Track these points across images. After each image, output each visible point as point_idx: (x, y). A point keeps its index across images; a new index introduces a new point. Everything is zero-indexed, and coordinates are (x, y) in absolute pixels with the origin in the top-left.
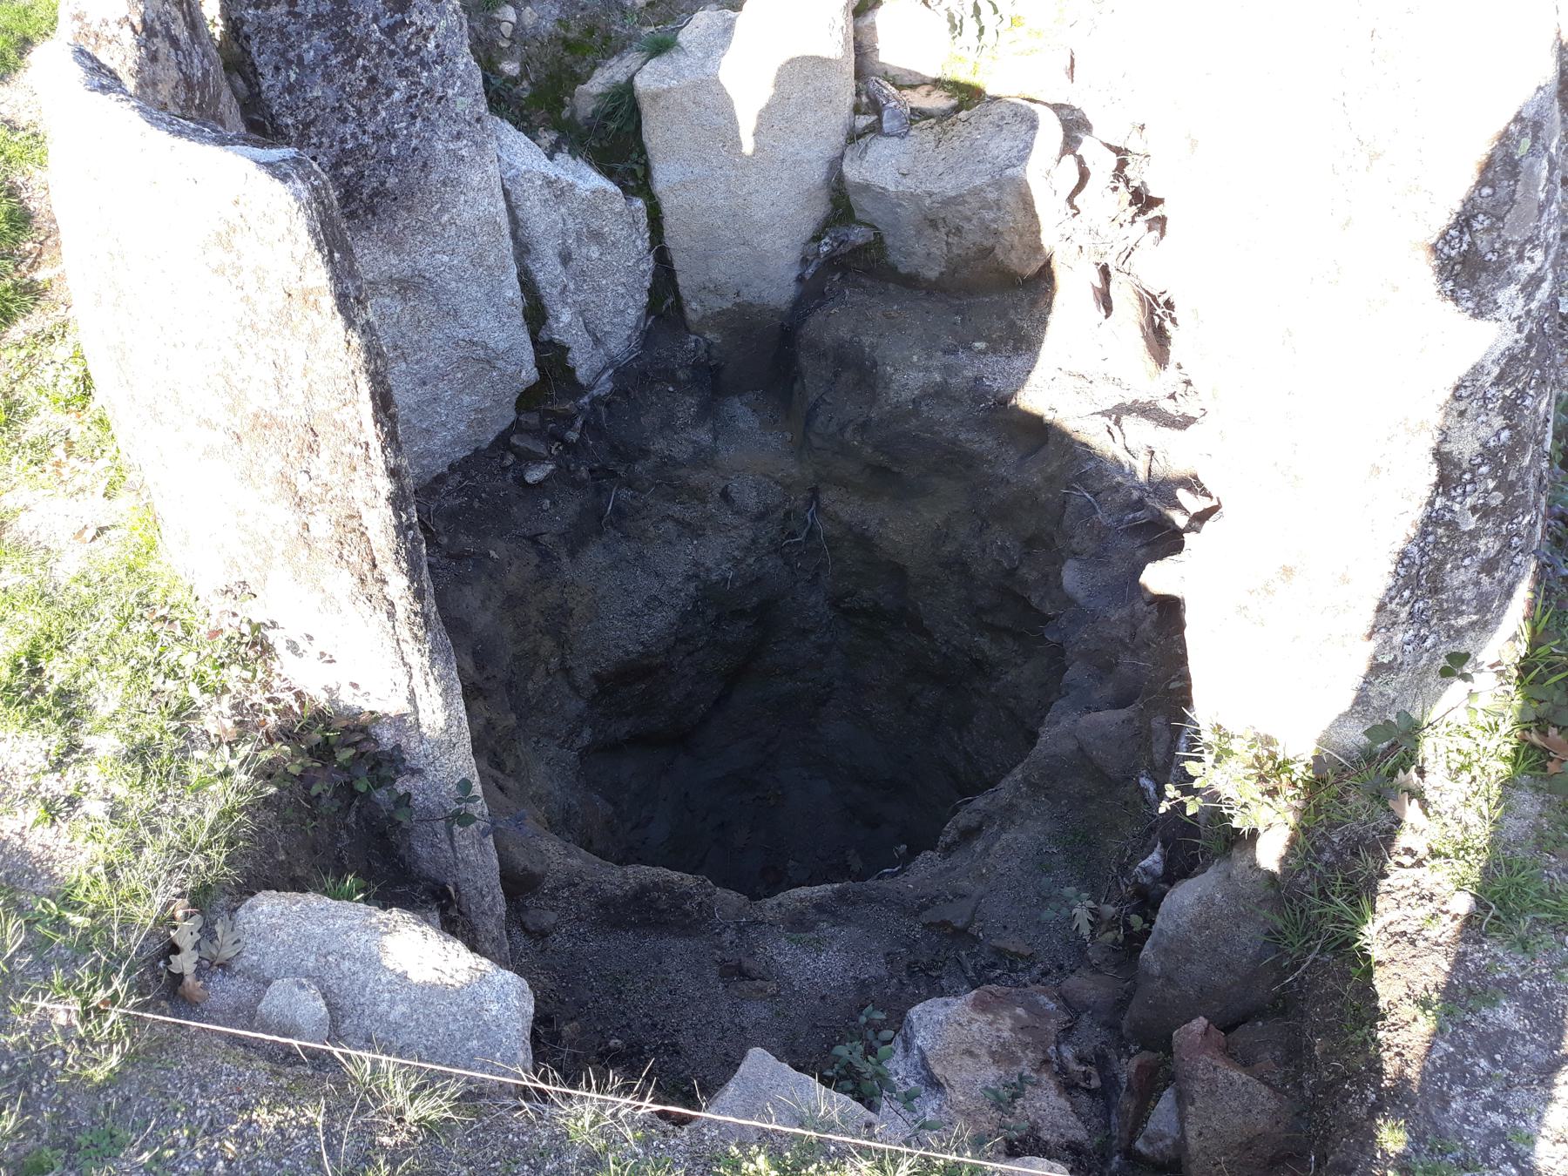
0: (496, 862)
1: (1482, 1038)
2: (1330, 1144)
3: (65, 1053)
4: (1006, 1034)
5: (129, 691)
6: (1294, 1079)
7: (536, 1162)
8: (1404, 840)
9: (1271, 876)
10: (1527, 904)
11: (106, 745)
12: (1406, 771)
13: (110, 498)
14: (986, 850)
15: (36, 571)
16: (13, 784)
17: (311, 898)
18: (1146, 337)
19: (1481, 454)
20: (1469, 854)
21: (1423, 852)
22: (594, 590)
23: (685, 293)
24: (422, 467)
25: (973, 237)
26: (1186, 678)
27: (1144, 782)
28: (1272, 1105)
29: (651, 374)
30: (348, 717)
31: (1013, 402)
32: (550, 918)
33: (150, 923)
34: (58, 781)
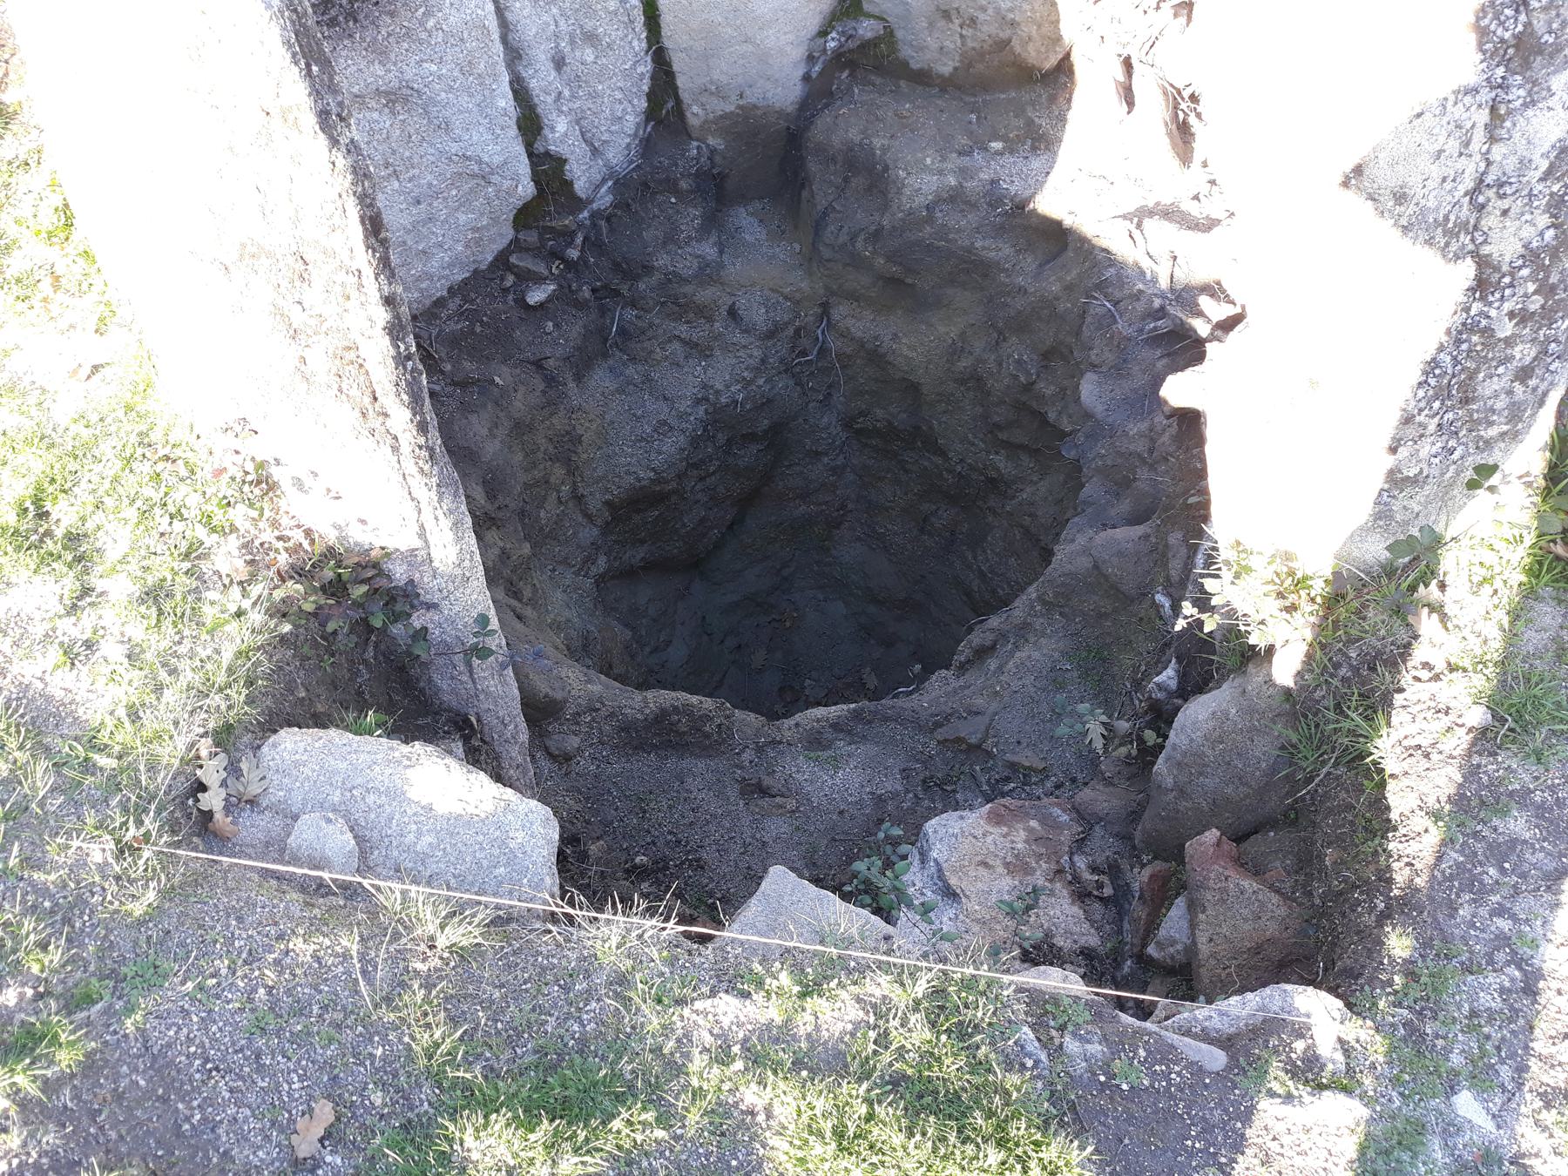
0: (516, 692)
1: (1492, 847)
2: (1339, 951)
3: (104, 889)
4: (1019, 846)
5: (138, 532)
6: (1304, 887)
7: (566, 983)
8: (1420, 653)
9: (1287, 692)
10: (1544, 716)
11: (119, 587)
12: (1426, 586)
13: (101, 334)
14: (1000, 669)
15: (34, 412)
16: (30, 628)
17: (333, 733)
18: (1170, 134)
19: (1523, 256)
20: (1487, 667)
21: (1440, 666)
22: (602, 416)
23: (685, 96)
24: (421, 291)
25: (989, 28)
26: (1204, 492)
27: (1159, 598)
28: (1283, 911)
29: (652, 185)
30: (359, 553)
31: (1031, 206)
32: (574, 742)
33: (176, 763)
34: (75, 624)
